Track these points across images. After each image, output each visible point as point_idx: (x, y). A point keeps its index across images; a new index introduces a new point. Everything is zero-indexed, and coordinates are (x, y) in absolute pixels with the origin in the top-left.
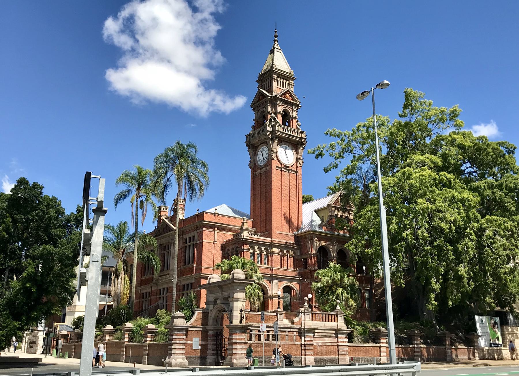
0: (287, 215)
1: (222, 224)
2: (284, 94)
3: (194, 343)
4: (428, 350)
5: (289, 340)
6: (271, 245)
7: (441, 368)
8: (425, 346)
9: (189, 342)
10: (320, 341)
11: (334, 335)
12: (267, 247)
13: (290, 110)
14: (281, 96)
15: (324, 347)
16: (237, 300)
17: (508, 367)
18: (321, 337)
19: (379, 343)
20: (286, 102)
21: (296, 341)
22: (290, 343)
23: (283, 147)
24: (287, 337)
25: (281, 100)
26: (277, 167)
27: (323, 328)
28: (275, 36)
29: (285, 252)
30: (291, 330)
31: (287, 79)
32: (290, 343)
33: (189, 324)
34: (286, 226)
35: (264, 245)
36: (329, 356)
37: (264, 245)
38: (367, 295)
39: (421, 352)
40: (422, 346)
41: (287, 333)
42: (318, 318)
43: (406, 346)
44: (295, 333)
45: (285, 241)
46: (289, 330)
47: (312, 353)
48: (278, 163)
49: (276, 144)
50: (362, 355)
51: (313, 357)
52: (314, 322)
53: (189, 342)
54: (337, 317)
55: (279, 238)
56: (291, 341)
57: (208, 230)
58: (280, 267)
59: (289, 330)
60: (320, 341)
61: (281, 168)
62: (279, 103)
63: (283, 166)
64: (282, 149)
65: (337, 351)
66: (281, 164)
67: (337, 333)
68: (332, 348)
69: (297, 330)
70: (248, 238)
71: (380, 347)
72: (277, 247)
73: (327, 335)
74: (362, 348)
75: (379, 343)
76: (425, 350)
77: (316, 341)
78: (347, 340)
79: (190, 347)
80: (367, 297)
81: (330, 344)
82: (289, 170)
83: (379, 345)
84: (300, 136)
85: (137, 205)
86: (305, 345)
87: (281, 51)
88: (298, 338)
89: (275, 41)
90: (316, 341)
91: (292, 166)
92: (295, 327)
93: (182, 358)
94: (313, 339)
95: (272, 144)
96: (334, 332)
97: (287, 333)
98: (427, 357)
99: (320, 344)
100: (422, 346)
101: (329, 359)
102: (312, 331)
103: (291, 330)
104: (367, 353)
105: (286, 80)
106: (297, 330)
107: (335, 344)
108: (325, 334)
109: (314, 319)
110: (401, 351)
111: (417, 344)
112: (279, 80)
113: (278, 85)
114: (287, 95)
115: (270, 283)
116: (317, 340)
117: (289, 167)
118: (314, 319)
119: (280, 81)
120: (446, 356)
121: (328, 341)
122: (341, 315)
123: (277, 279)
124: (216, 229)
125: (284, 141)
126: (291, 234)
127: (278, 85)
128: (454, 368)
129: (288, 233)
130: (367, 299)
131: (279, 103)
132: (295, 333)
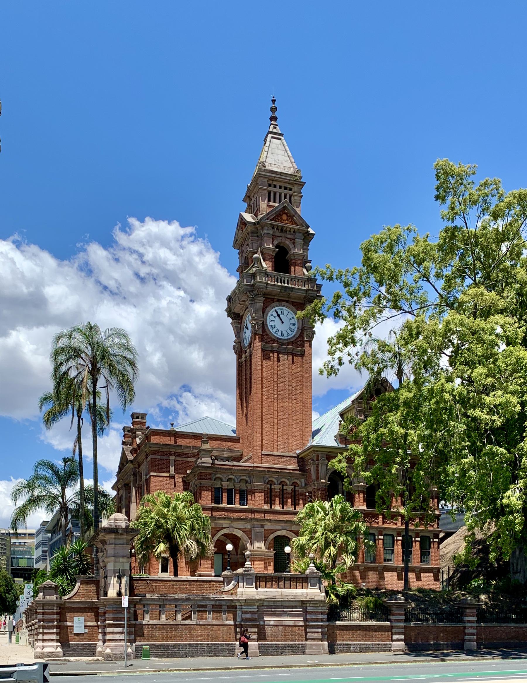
5: (213, 619)
19: (463, 621)
31: (289, 186)
99: (272, 623)
101: (289, 645)
125: (279, 300)
128: (138, 674)
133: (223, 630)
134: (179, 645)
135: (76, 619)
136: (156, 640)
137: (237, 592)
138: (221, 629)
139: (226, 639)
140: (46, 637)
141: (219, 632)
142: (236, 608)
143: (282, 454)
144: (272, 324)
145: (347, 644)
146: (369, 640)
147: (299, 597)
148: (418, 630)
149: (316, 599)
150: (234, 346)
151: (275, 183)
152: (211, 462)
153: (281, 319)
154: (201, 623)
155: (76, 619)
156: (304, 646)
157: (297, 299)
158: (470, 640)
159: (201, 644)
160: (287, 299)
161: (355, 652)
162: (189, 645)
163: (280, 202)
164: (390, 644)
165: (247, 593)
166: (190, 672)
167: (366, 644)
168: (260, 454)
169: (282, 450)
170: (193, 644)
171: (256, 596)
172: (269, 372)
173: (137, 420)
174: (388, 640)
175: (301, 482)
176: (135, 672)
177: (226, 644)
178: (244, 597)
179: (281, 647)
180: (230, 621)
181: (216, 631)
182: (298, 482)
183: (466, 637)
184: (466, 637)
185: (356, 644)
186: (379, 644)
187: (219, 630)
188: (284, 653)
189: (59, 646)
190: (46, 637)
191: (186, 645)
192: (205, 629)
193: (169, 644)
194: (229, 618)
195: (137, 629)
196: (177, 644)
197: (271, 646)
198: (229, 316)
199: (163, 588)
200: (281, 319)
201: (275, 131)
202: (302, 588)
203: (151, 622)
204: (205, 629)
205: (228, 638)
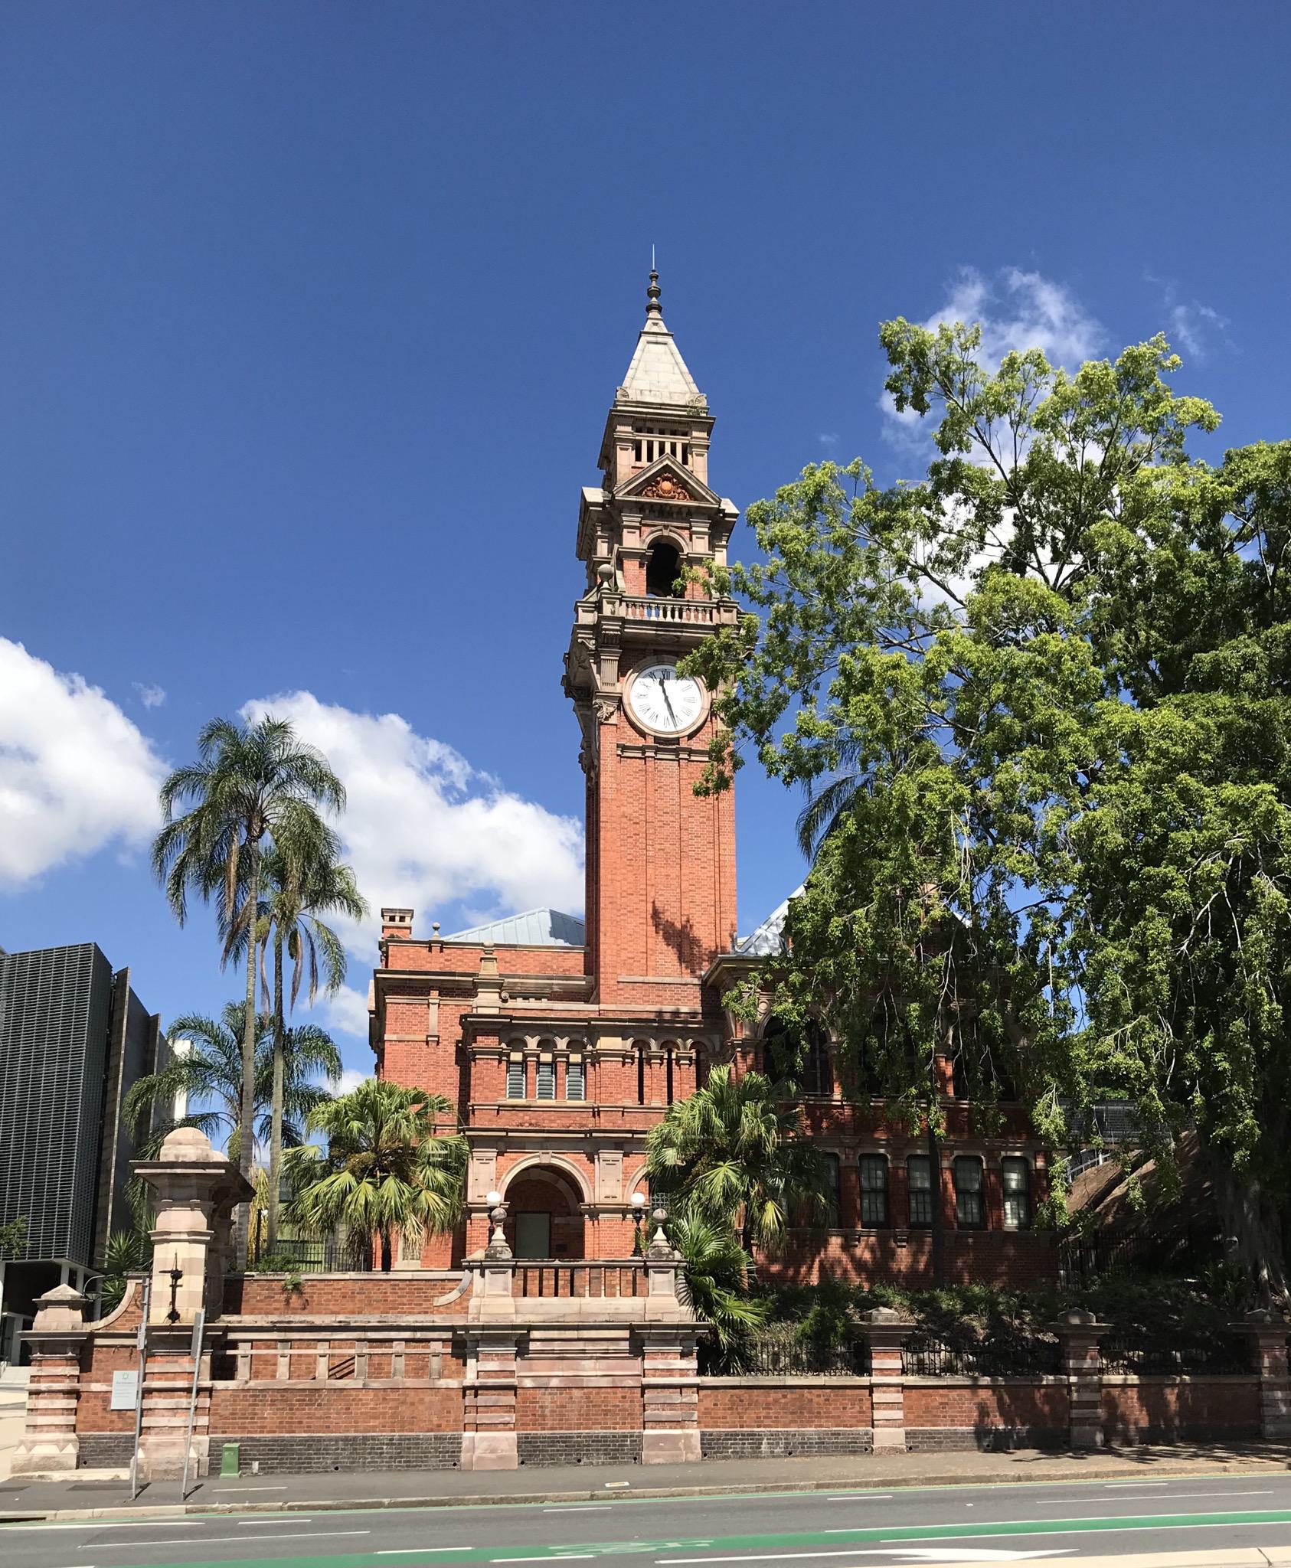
2: (652, 482)
4: (1151, 1397)
5: (407, 1374)
6: (592, 1030)
7: (1116, 1473)
8: (1133, 1379)
9: (95, 1387)
10: (556, 1373)
11: (625, 1345)
13: (681, 538)
14: (629, 493)
15: (576, 1393)
16: (166, 1238)
20: (663, 512)
21: (441, 1376)
22: (410, 1382)
23: (652, 675)
24: (400, 1363)
25: (640, 508)
26: (624, 748)
28: (651, 294)
29: (654, 1046)
30: (419, 1335)
31: (681, 428)
32: (410, 1382)
33: (98, 1325)
35: (562, 1031)
36: (598, 1431)
38: (1014, 1180)
40: (1116, 1379)
41: (398, 1347)
43: (1019, 1380)
47: (511, 1418)
49: (610, 668)
53: (95, 1387)
54: (647, 1274)
55: (633, 1001)
60: (556, 1373)
61: (643, 749)
62: (628, 519)
65: (638, 1409)
66: (643, 734)
67: (640, 1338)
68: (615, 1399)
69: (448, 1335)
70: (495, 1011)
71: (871, 1388)
72: (621, 1032)
73: (589, 1346)
74: (774, 1395)
75: (863, 1369)
76: (1133, 1394)
77: (525, 1374)
79: (99, 1403)
80: (1013, 1185)
82: (676, 752)
83: (865, 1380)
84: (716, 621)
86: (476, 1390)
87: (670, 340)
88: (454, 1363)
89: (649, 309)
90: (525, 1374)
91: (690, 737)
93: (56, 1442)
94: (513, 1366)
95: (599, 672)
96: (626, 1334)
98: (1144, 1423)
99: (554, 1383)
100: (1116, 1379)
101: (596, 1439)
103: (419, 1335)
104: (802, 1412)
106: (448, 1335)
107: (630, 1383)
108: (580, 1346)
109: (533, 1286)
111: (1078, 1372)
112: (644, 439)
113: (638, 458)
114: (666, 485)
116: (542, 1368)
117: (677, 741)
118: (533, 1286)
120: (1261, 1418)
121: (592, 1371)
122: (661, 1270)
124: (435, 993)
125: (656, 652)
126: (689, 979)
127: (638, 458)
128: (697, 1498)
129: (678, 980)
130: (1015, 1195)
131: (629, 519)
132: (436, 1347)
134: (319, 1440)
135: (117, 1375)
136: (262, 1429)
138: (427, 1399)
139: (439, 1426)
141: (421, 1408)
144: (642, 701)
145: (752, 1434)
146: (810, 1423)
147: (622, 1318)
149: (668, 1320)
152: (500, 1004)
154: (375, 1385)
155: (117, 1375)
156: (638, 1443)
162: (346, 1439)
164: (867, 1434)
167: (803, 1435)
168: (613, 982)
170: (355, 1438)
171: (514, 1317)
173: (391, 924)
177: (436, 1438)
178: (483, 1320)
181: (413, 1404)
185: (777, 1434)
187: (422, 1401)
188: (585, 1460)
189: (69, 1441)
191: (337, 1440)
192: (384, 1399)
196: (312, 1439)
198: (568, 694)
203: (252, 1384)
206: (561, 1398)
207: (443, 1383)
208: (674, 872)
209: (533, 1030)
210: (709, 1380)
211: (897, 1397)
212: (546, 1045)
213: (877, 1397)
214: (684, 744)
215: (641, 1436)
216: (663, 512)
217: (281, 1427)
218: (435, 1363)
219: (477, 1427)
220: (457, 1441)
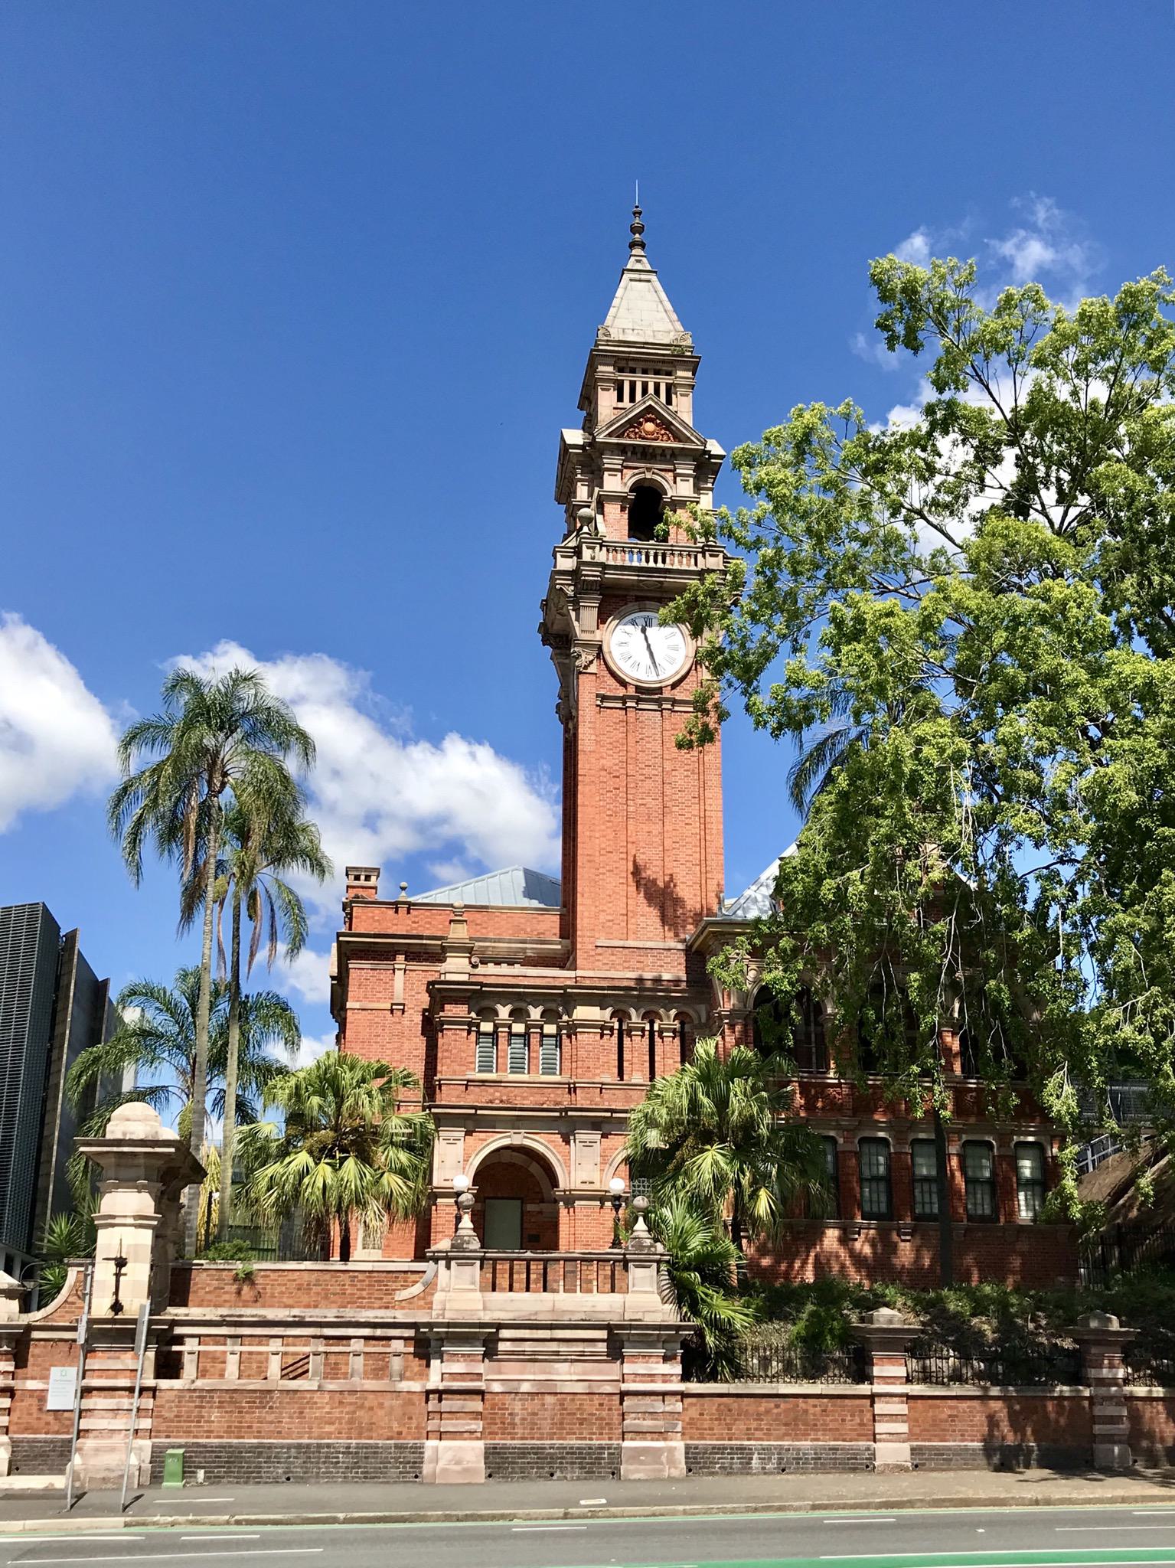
0: (653, 872)
1: (421, 937)
2: (634, 423)
3: (50, 1387)
5: (366, 1376)
6: (568, 999)
7: (1145, 1499)
8: (1159, 1391)
9: (31, 1385)
10: (527, 1377)
11: (602, 1347)
12: (553, 1006)
13: (665, 480)
14: (610, 435)
17: (392, 1539)
18: (533, 1358)
19: (867, 1378)
20: (646, 454)
21: (402, 1377)
22: (370, 1384)
23: (633, 623)
24: (358, 1363)
25: (622, 450)
27: (544, 1318)
30: (379, 1332)
32: (370, 1384)
33: (35, 1316)
34: (649, 916)
35: (536, 999)
37: (536, 999)
38: (1026, 1167)
39: (1135, 1417)
40: (1141, 1391)
41: (357, 1345)
42: (520, 1277)
44: (398, 1346)
45: (633, 975)
46: (367, 1332)
47: (478, 1425)
48: (612, 681)
49: (589, 615)
50: (768, 1436)
51: (480, 1445)
52: (499, 1297)
53: (31, 1385)
54: (626, 1269)
55: (613, 967)
56: (377, 1377)
57: (366, 964)
58: (610, 1077)
59: (367, 1332)
60: (527, 1377)
61: (623, 699)
62: (611, 461)
63: (631, 691)
64: (630, 628)
66: (623, 684)
67: (619, 1340)
68: (591, 1406)
69: (410, 1333)
70: (465, 978)
72: (600, 1001)
73: (563, 1348)
74: (765, 1404)
77: (495, 1377)
78: (677, 1369)
79: (35, 1402)
81: (580, 1388)
82: (659, 702)
83: (864, 1389)
85: (237, 908)
86: (440, 1394)
87: (653, 278)
88: (416, 1364)
89: (632, 245)
90: (495, 1377)
91: (674, 686)
92: (401, 1319)
94: (480, 1368)
95: (578, 619)
96: (603, 1334)
97: (357, 1345)
99: (525, 1387)
100: (1141, 1391)
102: (486, 1339)
103: (379, 1332)
104: (796, 1425)
105: (657, 372)
106: (410, 1333)
108: (553, 1347)
109: (503, 1281)
110: (1003, 1415)
112: (626, 379)
113: (620, 399)
114: (649, 426)
115: (568, 1143)
116: (512, 1371)
117: (660, 690)
118: (503, 1281)
119: (633, 385)
121: (567, 1375)
123: (595, 1124)
124: (401, 958)
125: (638, 599)
126: (672, 944)
127: (620, 399)
131: (611, 461)
132: (398, 1346)
133: (392, 1407)
134: (270, 1447)
135: (55, 1372)
136: (209, 1434)
137: (431, 1303)
138: (387, 1404)
139: (400, 1433)
140: (448, 1425)
142: (429, 1346)
143: (649, 944)
145: (742, 1448)
146: (805, 1436)
148: (950, 1407)
149: (649, 1320)
150: (558, 706)
151: (631, 364)
153: (646, 639)
155: (55, 1372)
157: (655, 591)
158: (1111, 1439)
159: (328, 1446)
160: (658, 595)
161: (765, 1472)
162: (299, 1447)
163: (632, 399)
164: (868, 1449)
165: (457, 1306)
166: (336, 1526)
168: (591, 947)
169: (650, 935)
172: (616, 756)
173: (356, 883)
174: (861, 1436)
175: (697, 1012)
176: (346, 1521)
177: (396, 1446)
179: (552, 1456)
180: (411, 1383)
181: (371, 1409)
182: (691, 1012)
183: (1098, 1429)
184: (1098, 1429)
186: (835, 1449)
187: (381, 1405)
188: (558, 1474)
190: (448, 1425)
191: (289, 1447)
192: (341, 1403)
193: (243, 1446)
194: (408, 1374)
195: (159, 1401)
197: (523, 1452)
199: (282, 1293)
200: (646, 639)
201: (639, 266)
202: (613, 1291)
203: (199, 1383)
204: (341, 1403)
205: (405, 1431)
206: (533, 1405)
207: (405, 1386)
208: (656, 828)
209: (504, 997)
210: (694, 1387)
211: (902, 1408)
212: (518, 1014)
213: (880, 1408)
214: (667, 694)
215: (619, 1448)
216: (646, 454)
217: (229, 1432)
218: (396, 1364)
219: (441, 1435)
220: (418, 1450)
